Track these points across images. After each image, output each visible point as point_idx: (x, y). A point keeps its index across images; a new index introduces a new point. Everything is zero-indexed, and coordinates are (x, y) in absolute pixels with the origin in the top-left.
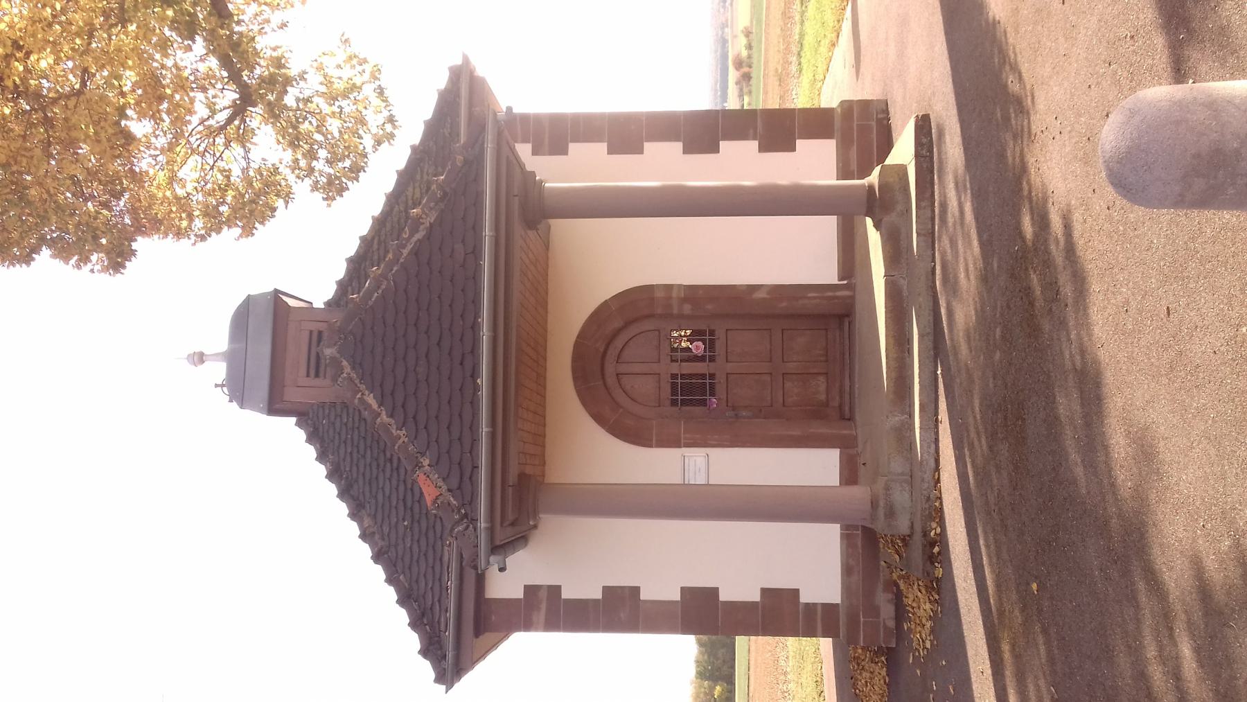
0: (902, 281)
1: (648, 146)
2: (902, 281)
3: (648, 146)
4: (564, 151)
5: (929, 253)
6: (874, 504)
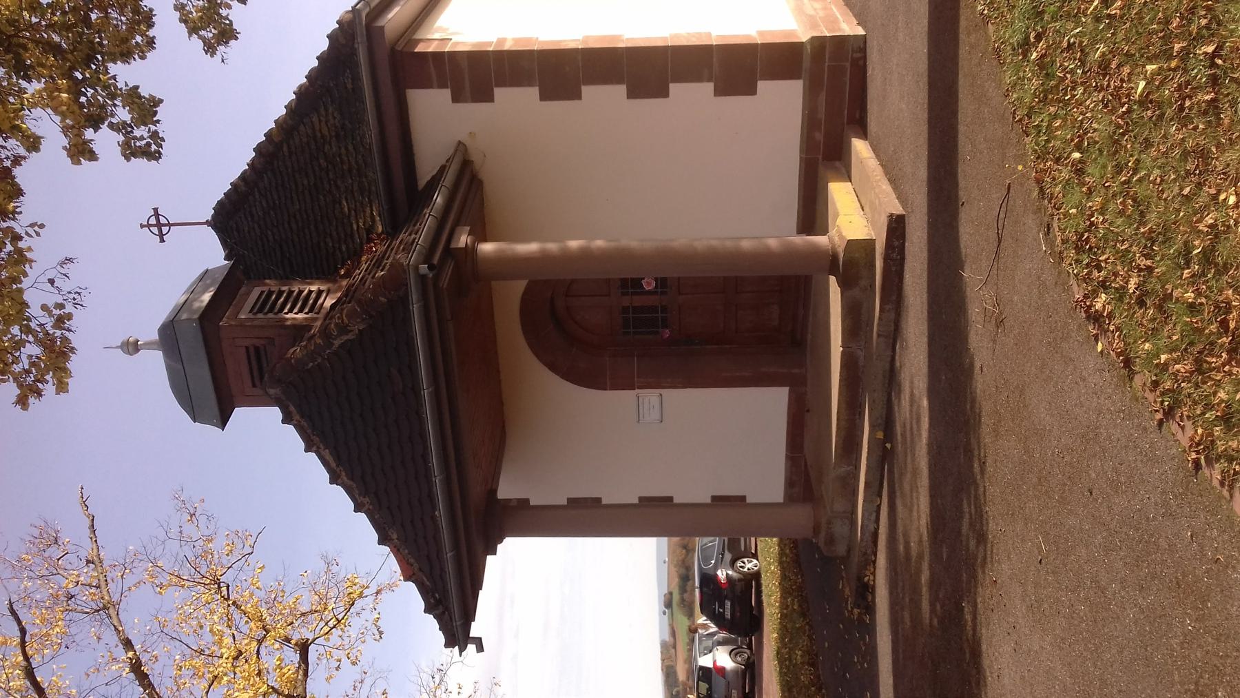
0: (859, 352)
1: (586, 90)
2: (859, 352)
3: (586, 90)
4: (489, 98)
5: (889, 353)
6: (816, 530)
